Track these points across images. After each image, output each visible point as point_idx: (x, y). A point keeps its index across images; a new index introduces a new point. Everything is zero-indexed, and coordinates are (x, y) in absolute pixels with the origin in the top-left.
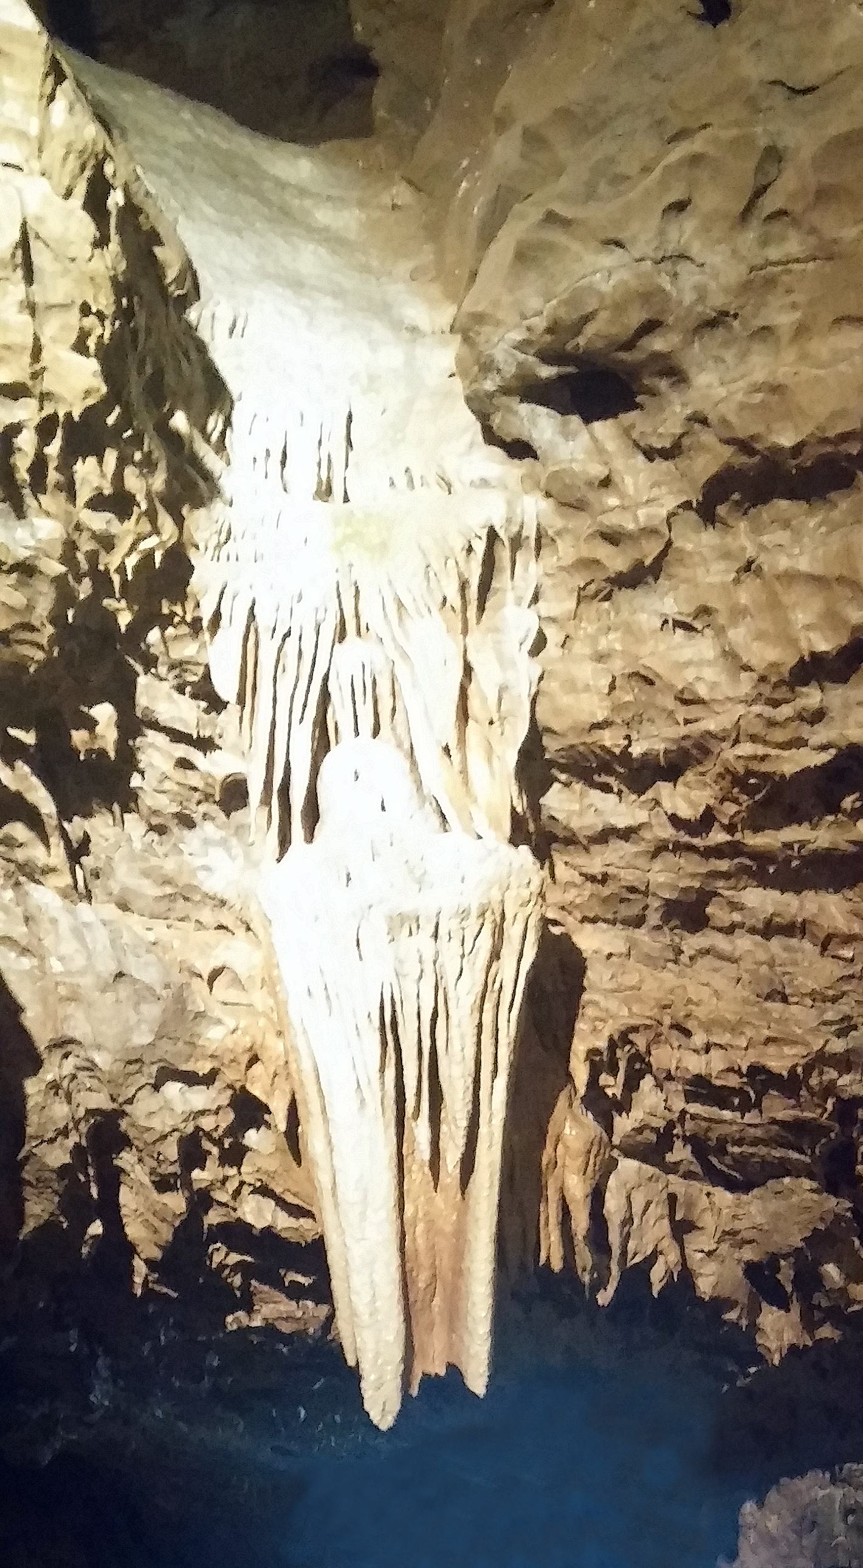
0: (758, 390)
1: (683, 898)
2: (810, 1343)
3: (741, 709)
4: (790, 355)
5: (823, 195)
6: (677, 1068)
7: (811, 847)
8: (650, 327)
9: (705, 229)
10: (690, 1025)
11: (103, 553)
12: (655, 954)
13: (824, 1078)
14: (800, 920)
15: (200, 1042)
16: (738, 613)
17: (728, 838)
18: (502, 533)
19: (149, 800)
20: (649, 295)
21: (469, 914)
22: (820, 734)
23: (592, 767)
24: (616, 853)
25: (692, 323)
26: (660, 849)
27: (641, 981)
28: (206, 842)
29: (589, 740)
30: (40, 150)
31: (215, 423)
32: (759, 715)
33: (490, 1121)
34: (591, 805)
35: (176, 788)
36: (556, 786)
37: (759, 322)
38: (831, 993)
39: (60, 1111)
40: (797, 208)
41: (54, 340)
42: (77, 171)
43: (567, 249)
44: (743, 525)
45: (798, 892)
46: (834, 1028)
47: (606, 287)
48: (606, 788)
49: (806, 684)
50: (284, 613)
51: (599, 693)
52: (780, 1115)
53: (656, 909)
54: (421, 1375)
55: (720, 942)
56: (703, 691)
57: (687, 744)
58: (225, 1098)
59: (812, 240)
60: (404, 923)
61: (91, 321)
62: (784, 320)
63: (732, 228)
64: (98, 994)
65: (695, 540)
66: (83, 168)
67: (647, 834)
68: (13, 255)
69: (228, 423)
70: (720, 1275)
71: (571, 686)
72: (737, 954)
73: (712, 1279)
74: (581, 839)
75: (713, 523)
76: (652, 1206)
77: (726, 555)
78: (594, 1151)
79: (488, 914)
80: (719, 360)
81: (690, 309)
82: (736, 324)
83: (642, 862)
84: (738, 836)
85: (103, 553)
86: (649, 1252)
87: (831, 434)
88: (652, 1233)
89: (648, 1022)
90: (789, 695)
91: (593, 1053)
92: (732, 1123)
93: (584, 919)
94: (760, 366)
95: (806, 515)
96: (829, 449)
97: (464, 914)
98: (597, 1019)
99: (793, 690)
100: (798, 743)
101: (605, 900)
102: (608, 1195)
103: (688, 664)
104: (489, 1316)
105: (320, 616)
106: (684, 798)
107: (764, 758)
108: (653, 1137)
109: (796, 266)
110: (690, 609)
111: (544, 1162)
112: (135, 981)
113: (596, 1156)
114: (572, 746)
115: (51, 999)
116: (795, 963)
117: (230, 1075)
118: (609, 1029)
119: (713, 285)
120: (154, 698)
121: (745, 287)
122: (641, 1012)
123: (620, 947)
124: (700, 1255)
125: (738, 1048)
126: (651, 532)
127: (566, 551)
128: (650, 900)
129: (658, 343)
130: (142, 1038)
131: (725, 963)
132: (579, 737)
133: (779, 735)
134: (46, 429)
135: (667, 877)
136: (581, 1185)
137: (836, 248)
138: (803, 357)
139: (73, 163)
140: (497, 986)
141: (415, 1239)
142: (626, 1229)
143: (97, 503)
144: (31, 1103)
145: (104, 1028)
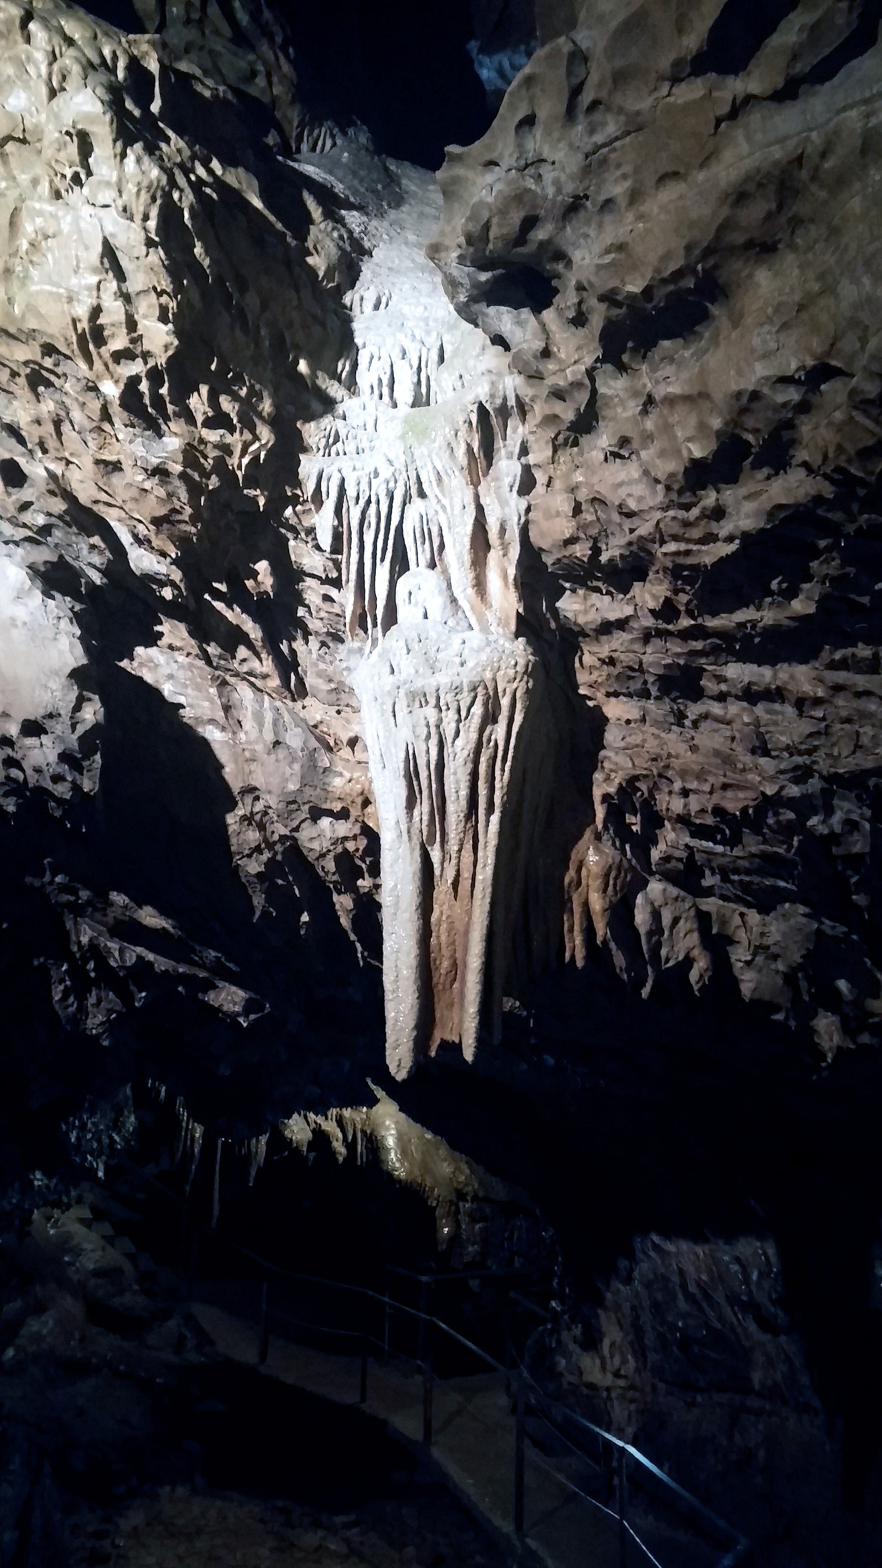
0: (608, 251)
1: (668, 673)
2: (852, 1046)
3: (658, 515)
4: (630, 217)
5: (620, 78)
6: (668, 809)
7: (760, 625)
8: (530, 223)
9: (548, 133)
10: (670, 774)
11: (227, 458)
12: (661, 719)
13: (781, 818)
14: (774, 687)
15: (330, 789)
16: (648, 438)
17: (693, 622)
18: (487, 406)
19: (314, 624)
20: (520, 197)
21: (462, 689)
22: (725, 528)
23: (588, 574)
24: (618, 642)
25: (558, 212)
26: (647, 637)
27: (644, 740)
28: (351, 651)
29: (567, 554)
30: (120, 192)
31: (343, 367)
32: (674, 518)
33: (486, 847)
34: (593, 605)
35: (326, 615)
36: (568, 593)
37: (602, 198)
38: (803, 747)
39: (253, 836)
40: (603, 95)
41: (145, 317)
42: (149, 201)
43: (467, 178)
44: (644, 367)
45: (773, 665)
46: (788, 776)
47: (490, 199)
48: (598, 590)
49: (704, 488)
50: (364, 486)
51: (567, 516)
52: (753, 850)
53: (653, 683)
54: (439, 1041)
55: (716, 709)
56: (633, 505)
57: (634, 548)
58: (357, 830)
59: (622, 118)
60: (419, 698)
61: (164, 299)
62: (618, 189)
63: (564, 126)
64: (265, 756)
65: (612, 386)
66: (154, 199)
67: (634, 624)
68: (102, 263)
69: (355, 366)
70: (759, 983)
71: (550, 515)
72: (729, 717)
73: (751, 985)
74: (588, 632)
75: (626, 370)
76: (682, 922)
77: (635, 394)
78: (613, 874)
79: (480, 689)
80: (586, 236)
81: (554, 200)
82: (588, 203)
83: (637, 647)
84: (700, 620)
85: (227, 458)
86: (680, 958)
87: (666, 274)
88: (684, 942)
89: (644, 772)
90: (694, 499)
91: (606, 798)
92: (723, 855)
93: (608, 695)
94: (613, 231)
95: (684, 348)
96: (671, 288)
97: (457, 690)
98: (612, 771)
99: (695, 494)
100: (710, 538)
101: (618, 677)
102: (636, 912)
103: (620, 485)
104: (478, 1000)
105: (391, 485)
106: (650, 593)
107: (687, 553)
108: (681, 866)
109: (617, 144)
110: (614, 441)
111: (567, 880)
112: (288, 747)
113: (616, 878)
114: (559, 560)
115: (241, 760)
116: (776, 723)
117: (354, 812)
118: (618, 779)
119: (563, 178)
120: (301, 555)
121: (587, 171)
122: (642, 765)
123: (635, 714)
124: (742, 964)
125: (704, 792)
126: (576, 385)
127: (539, 411)
128: (646, 676)
129: (541, 234)
130: (292, 787)
131: (721, 726)
132: (559, 551)
133: (696, 533)
134: (155, 376)
135: (656, 657)
136: (601, 901)
137: (639, 119)
138: (641, 217)
139: (145, 196)
140: (492, 744)
141: (438, 937)
142: (654, 939)
143: (209, 423)
144: (231, 829)
145: (271, 779)
